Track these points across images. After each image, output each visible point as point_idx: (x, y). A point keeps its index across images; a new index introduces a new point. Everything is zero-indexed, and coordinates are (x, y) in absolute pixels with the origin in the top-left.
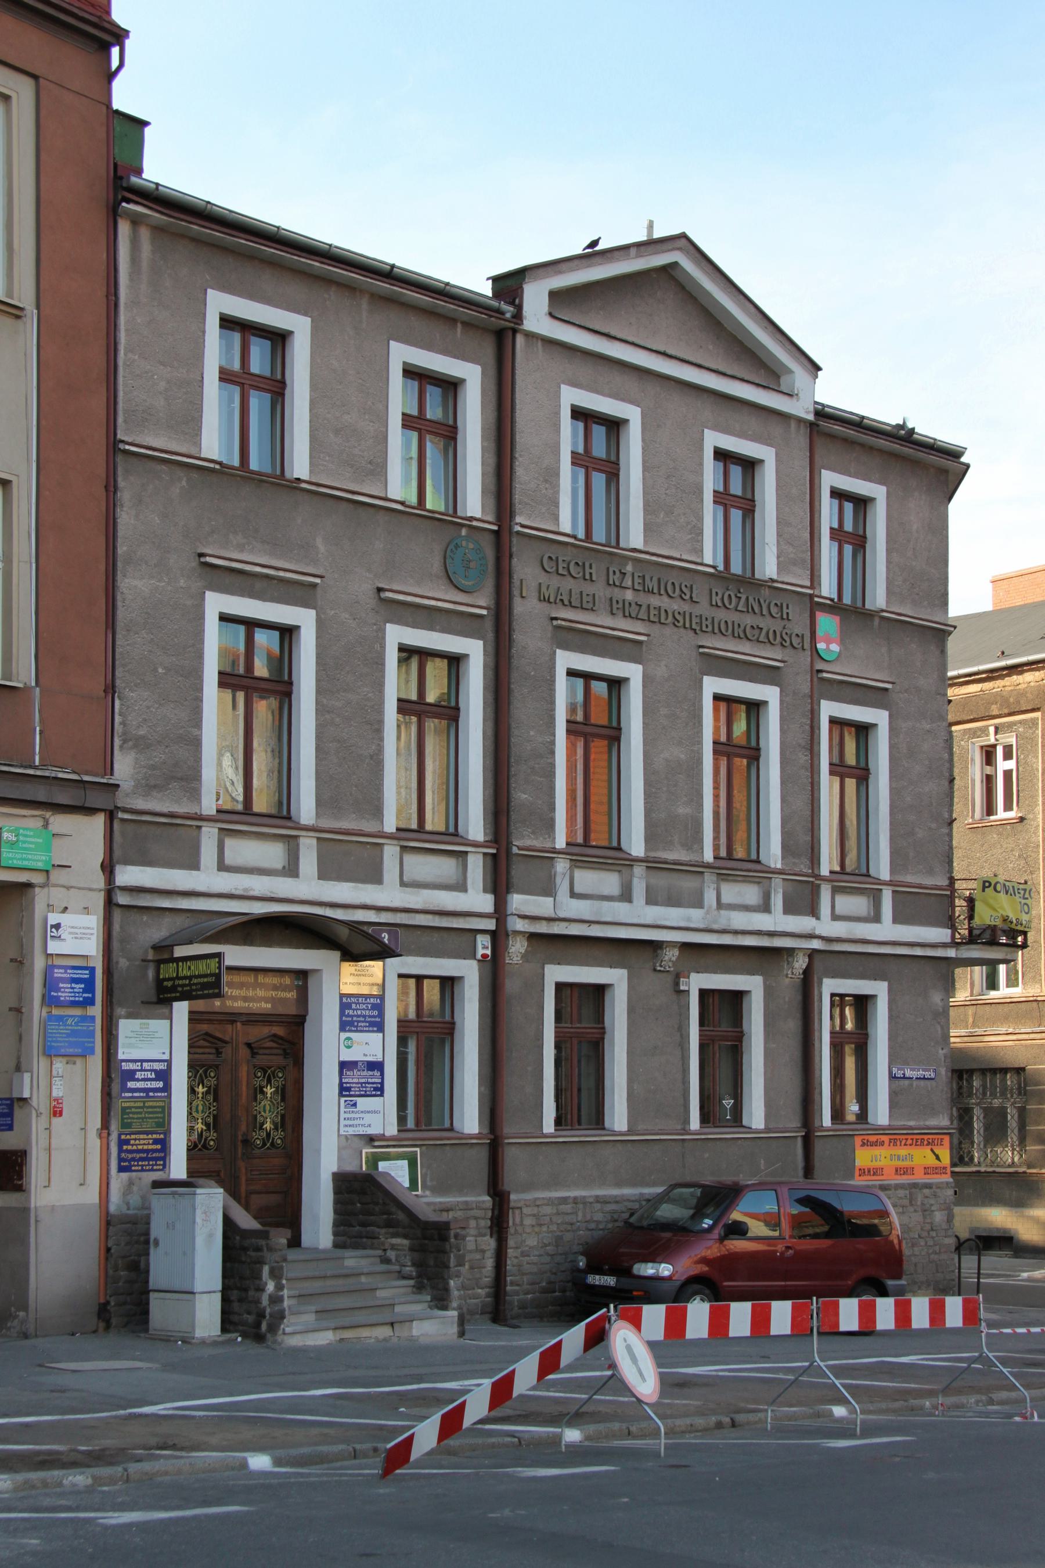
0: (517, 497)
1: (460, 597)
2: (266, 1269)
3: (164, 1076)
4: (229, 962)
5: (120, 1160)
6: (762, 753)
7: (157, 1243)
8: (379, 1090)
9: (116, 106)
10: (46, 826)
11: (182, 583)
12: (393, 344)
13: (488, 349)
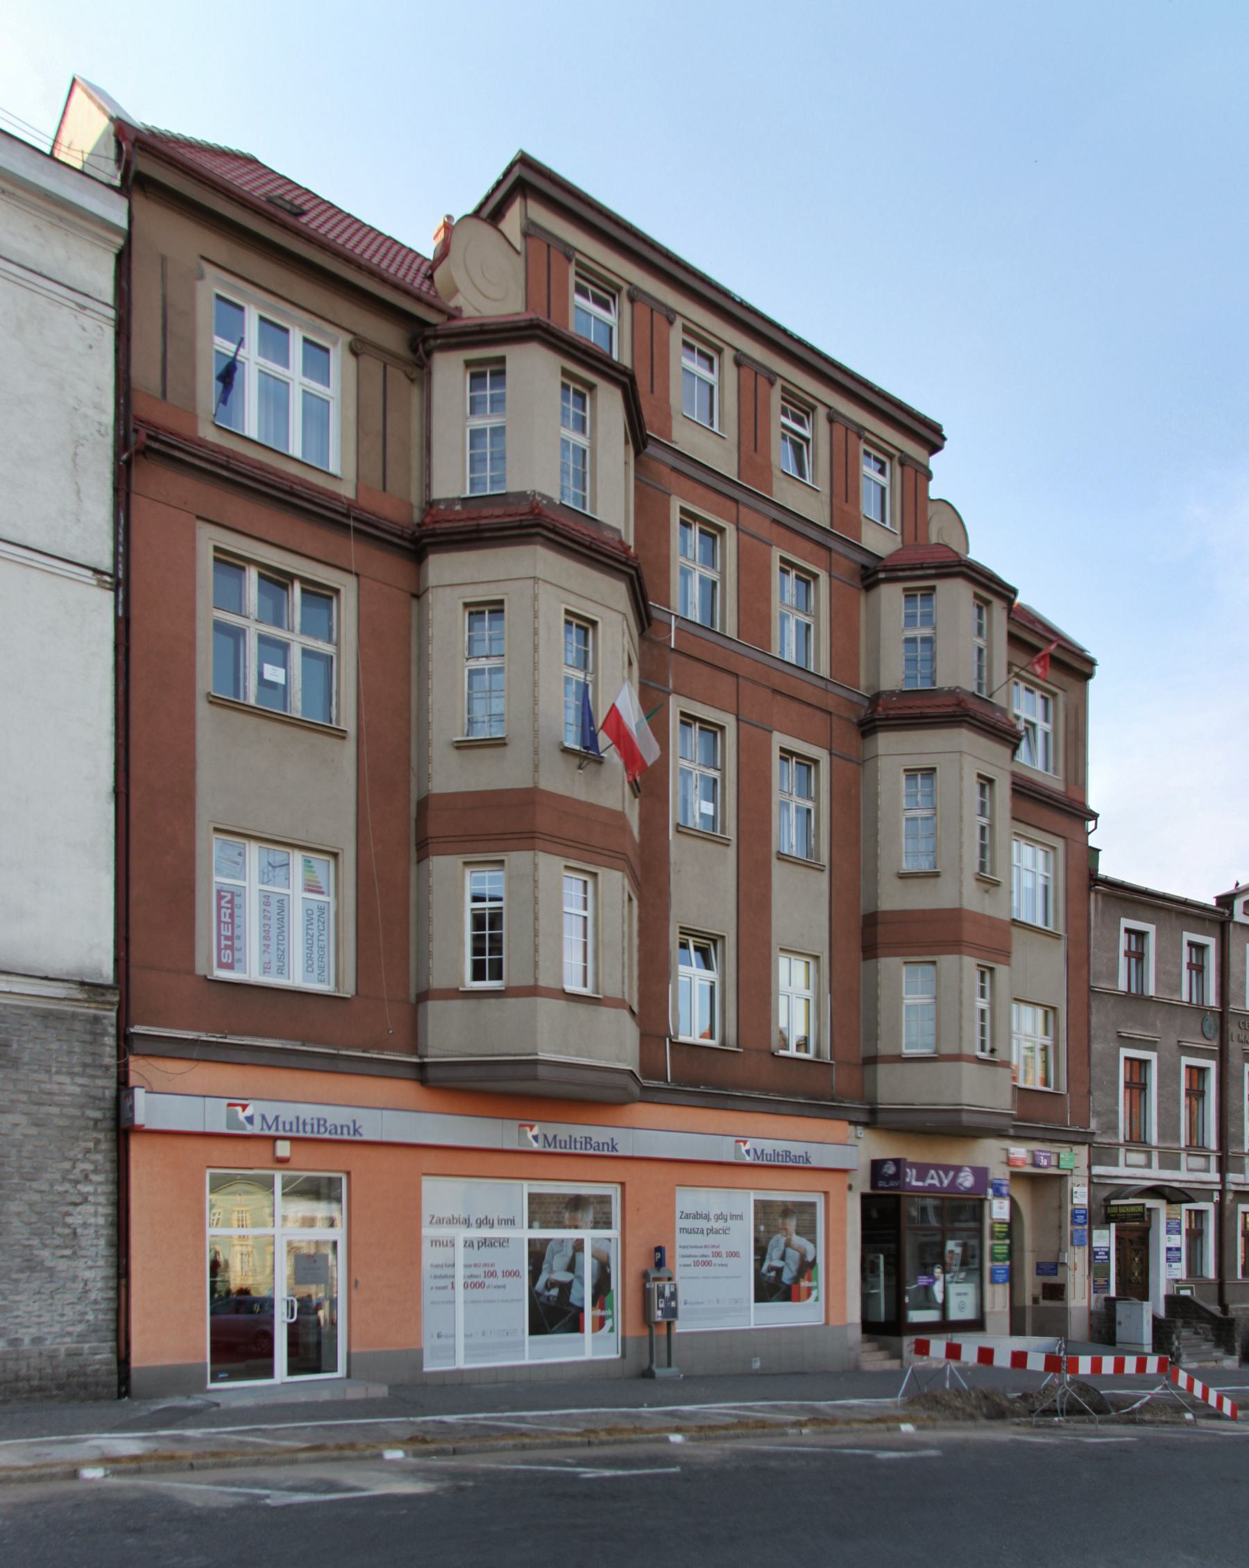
0: (1231, 996)
1: (1207, 1042)
2: (1174, 1336)
3: (1108, 1253)
4: (1147, 1206)
5: (1094, 1288)
6: (1148, 1087)
7: (1120, 1323)
8: (1179, 1260)
9: (1090, 845)
10: (1071, 1151)
11: (1112, 1045)
12: (1184, 933)
13: (1217, 931)
